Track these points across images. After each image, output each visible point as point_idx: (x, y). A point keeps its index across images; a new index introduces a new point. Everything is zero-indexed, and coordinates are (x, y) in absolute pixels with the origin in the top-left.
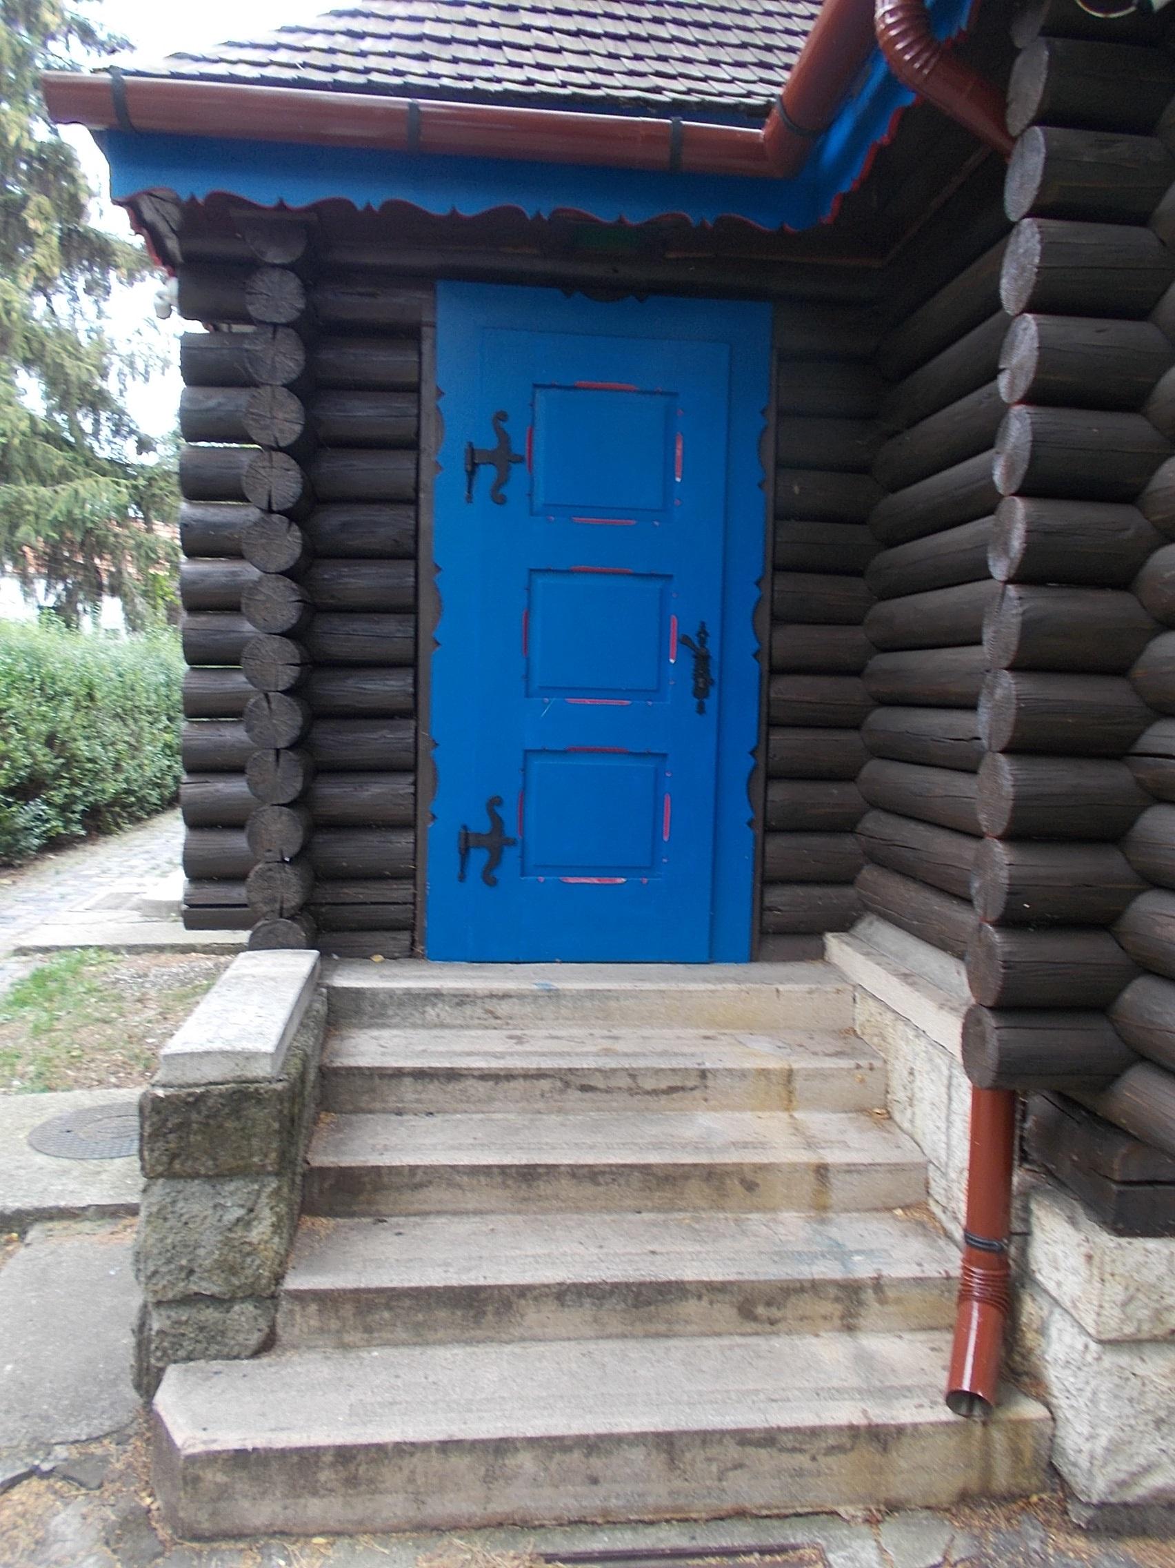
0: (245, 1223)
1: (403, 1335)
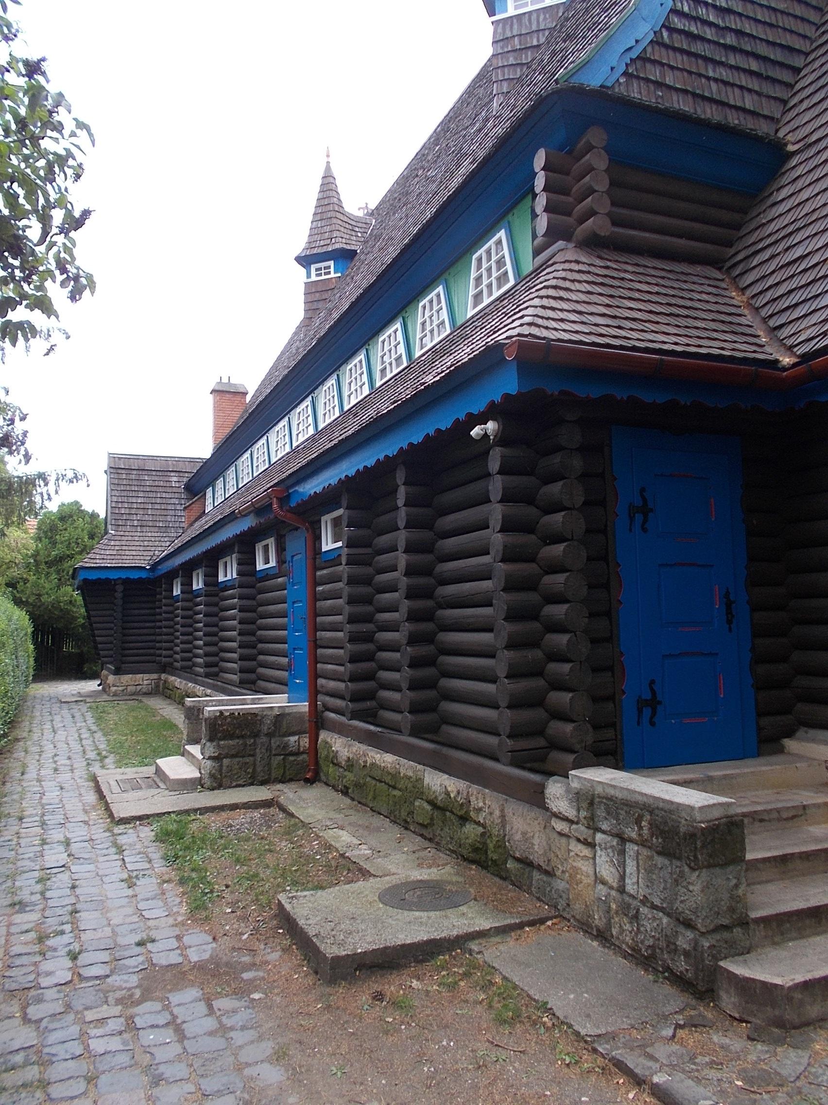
0: (736, 886)
1: (794, 934)
